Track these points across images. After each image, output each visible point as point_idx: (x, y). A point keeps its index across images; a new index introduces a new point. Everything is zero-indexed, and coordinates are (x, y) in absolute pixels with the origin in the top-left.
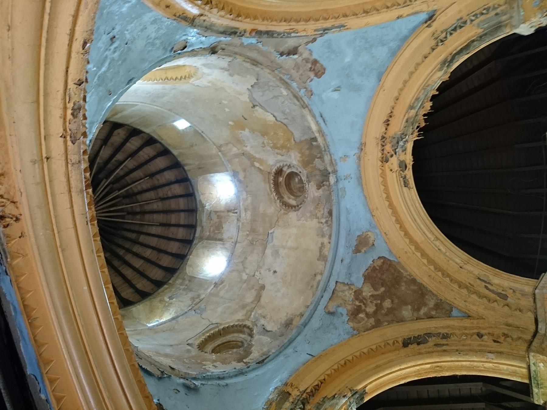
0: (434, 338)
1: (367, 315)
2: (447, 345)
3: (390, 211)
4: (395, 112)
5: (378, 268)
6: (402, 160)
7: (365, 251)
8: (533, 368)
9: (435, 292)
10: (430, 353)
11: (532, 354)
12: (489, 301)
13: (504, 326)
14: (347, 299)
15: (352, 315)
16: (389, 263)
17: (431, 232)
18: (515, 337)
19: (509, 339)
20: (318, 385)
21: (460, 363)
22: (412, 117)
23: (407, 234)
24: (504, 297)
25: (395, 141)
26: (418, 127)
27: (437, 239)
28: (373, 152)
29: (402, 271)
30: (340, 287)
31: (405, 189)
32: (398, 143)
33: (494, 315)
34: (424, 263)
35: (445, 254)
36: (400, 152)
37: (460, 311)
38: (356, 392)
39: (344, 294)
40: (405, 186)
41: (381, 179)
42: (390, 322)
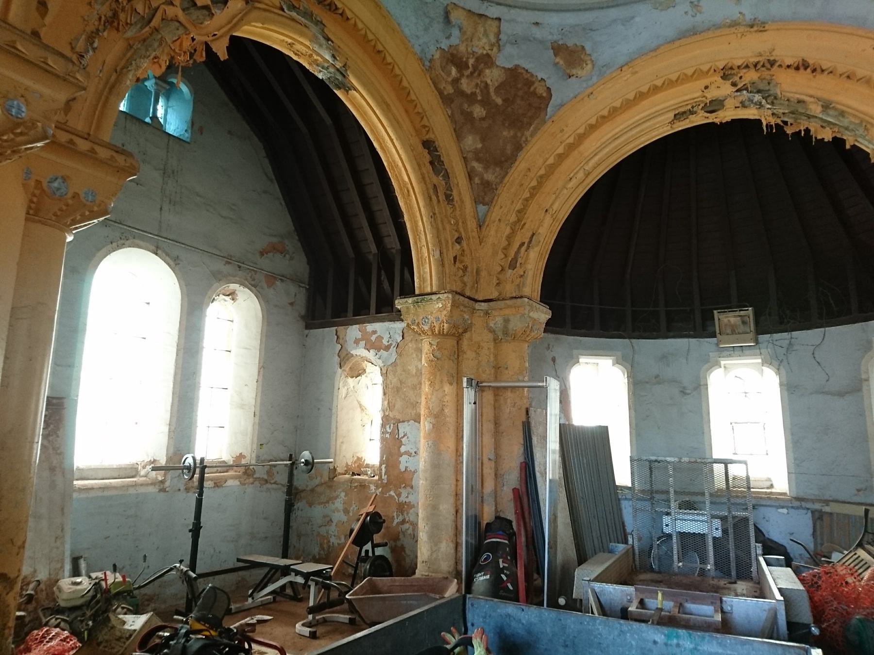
0: (443, 183)
1: (456, 81)
2: (439, 201)
3: (631, 96)
4: (822, 78)
5: (532, 89)
6: (726, 103)
7: (558, 63)
8: (434, 297)
9: (507, 179)
10: (423, 179)
11: (450, 296)
12: (505, 249)
13: (475, 266)
14: (475, 42)
15: (452, 55)
16: (543, 106)
17: (598, 164)
18: (465, 279)
19: (461, 273)
20: (337, 8)
21: (419, 218)
22: (807, 109)
23: (592, 128)
24: (513, 265)
25: (761, 86)
26: (786, 123)
27: (587, 175)
28: (742, 49)
29: (531, 129)
30: (492, 27)
31: (671, 115)
32: (759, 91)
33: (488, 254)
34: (547, 159)
35: (564, 187)
36: (741, 99)
37: (486, 216)
38: (344, 76)
39: (481, 36)
40: (675, 115)
41: (690, 72)
42: (452, 117)
